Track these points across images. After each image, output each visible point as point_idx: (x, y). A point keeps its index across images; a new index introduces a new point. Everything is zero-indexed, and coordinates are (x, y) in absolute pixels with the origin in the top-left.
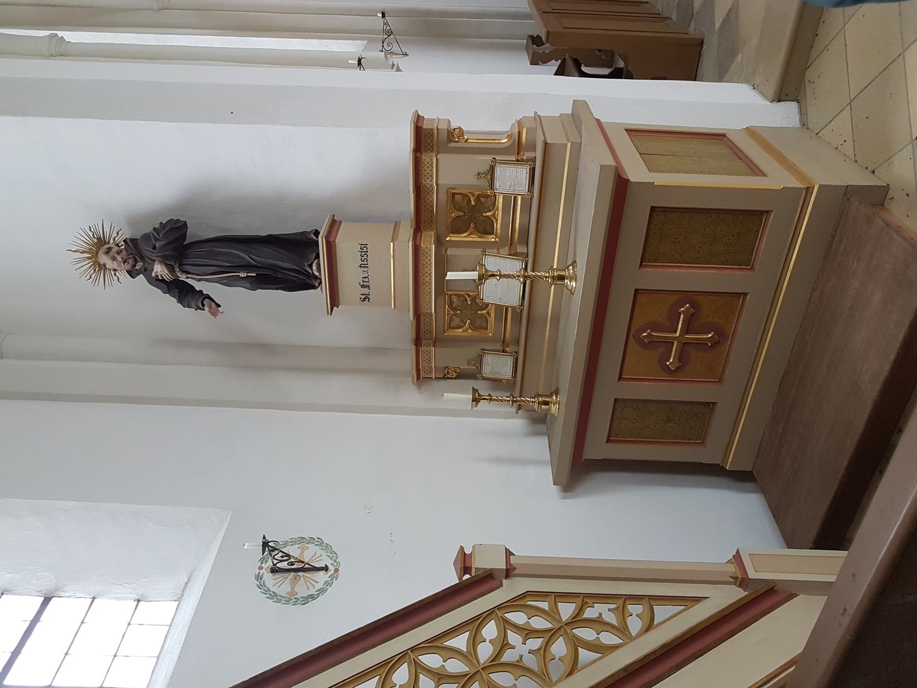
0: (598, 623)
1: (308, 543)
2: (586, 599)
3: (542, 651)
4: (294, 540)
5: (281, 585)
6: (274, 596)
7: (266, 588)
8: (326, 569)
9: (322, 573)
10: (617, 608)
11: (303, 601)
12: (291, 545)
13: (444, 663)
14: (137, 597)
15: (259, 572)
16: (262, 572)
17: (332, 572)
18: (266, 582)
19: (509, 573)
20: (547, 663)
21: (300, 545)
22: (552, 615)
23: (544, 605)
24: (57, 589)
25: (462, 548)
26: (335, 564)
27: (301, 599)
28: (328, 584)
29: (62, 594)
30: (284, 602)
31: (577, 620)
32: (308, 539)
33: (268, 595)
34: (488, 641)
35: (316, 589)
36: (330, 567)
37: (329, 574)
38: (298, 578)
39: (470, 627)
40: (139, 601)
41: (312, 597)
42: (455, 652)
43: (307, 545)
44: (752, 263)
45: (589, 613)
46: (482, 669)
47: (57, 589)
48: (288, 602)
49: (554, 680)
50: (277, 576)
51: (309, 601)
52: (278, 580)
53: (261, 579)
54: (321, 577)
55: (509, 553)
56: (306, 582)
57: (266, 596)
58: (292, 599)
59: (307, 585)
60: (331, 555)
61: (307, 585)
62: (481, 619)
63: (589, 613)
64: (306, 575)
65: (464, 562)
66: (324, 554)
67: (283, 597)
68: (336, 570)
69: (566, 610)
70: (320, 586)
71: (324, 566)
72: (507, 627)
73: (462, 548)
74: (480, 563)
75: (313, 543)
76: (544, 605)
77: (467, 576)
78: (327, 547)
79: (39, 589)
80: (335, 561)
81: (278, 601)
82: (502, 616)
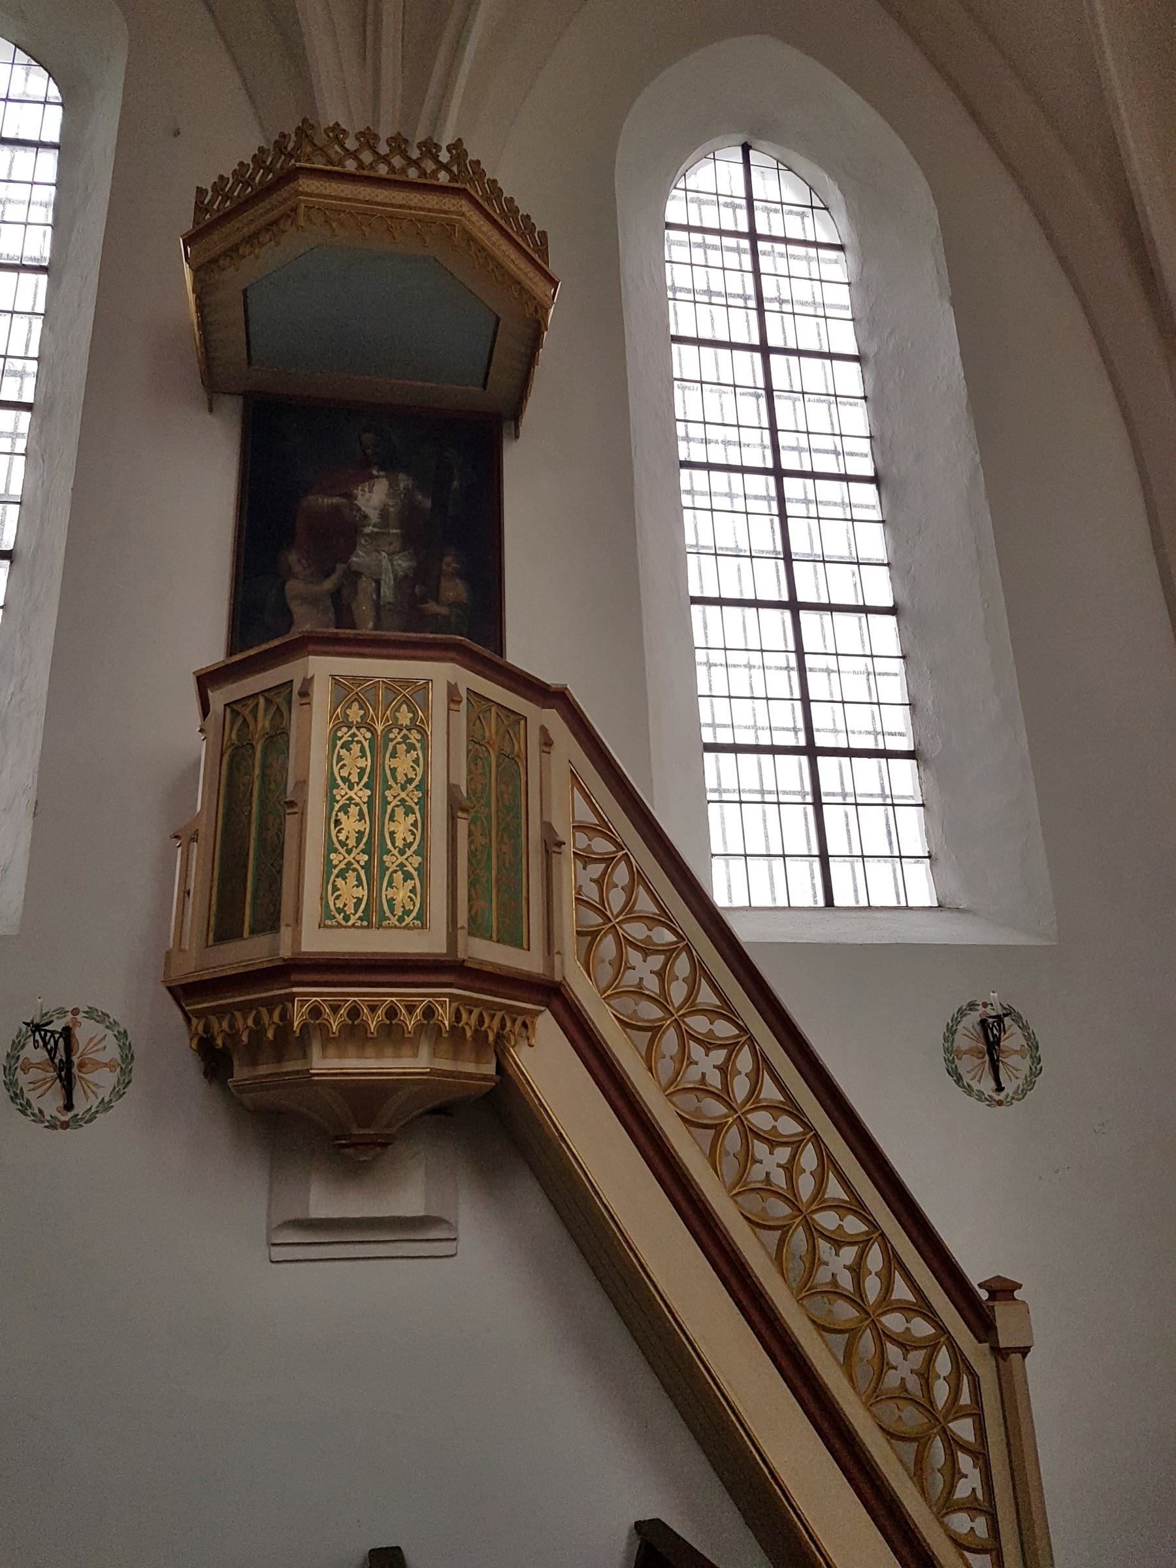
0: (954, 1474)
1: (1031, 1057)
2: (981, 1456)
3: (904, 1395)
4: (1032, 1036)
5: (967, 1037)
6: (951, 1031)
7: (959, 1019)
8: (1000, 1089)
9: (993, 1085)
10: (976, 1499)
11: (952, 1069)
12: (1024, 1035)
13: (873, 1273)
14: (933, 854)
15: (979, 1005)
16: (980, 1008)
17: (997, 1098)
18: (968, 1017)
19: (1000, 1353)
20: (894, 1400)
21: (1026, 1046)
22: (954, 1410)
23: (965, 1399)
24: (925, 761)
25: (1020, 1286)
26: (1009, 1099)
27: (954, 1066)
28: (980, 1096)
29: (921, 769)
30: (946, 1045)
31: (953, 1444)
32: (1037, 1055)
33: (951, 1024)
34: (909, 1325)
35: (970, 1082)
36: (1003, 1094)
37: (994, 1095)
38: (980, 1055)
39: (921, 1303)
40: (929, 857)
41: (959, 1080)
42: (888, 1287)
43: (1028, 1057)
44: (767, 1472)
45: (965, 1462)
46: (873, 1320)
47: (925, 761)
48: (946, 1050)
49: (873, 1409)
50: (978, 1028)
51: (953, 1077)
52: (974, 1032)
53: (970, 1010)
54: (987, 1086)
55: (1024, 1351)
56: (976, 1067)
57: (950, 1022)
58: (952, 1054)
59: (973, 1070)
60: (1020, 1092)
61: (973, 1070)
62: (930, 1314)
63: (965, 1462)
64: (987, 1064)
65: (1003, 1290)
66: (1020, 1082)
67: (952, 1045)
68: (1000, 1103)
69: (964, 1429)
70: (975, 1086)
71: (1003, 1086)
72: (929, 1349)
73: (1020, 1286)
74: (1002, 1313)
75: (1033, 1063)
76: (965, 1399)
77: (984, 1295)
78: (1030, 1084)
79: (922, 742)
80: (1013, 1098)
81: (946, 1040)
82: (941, 1343)
